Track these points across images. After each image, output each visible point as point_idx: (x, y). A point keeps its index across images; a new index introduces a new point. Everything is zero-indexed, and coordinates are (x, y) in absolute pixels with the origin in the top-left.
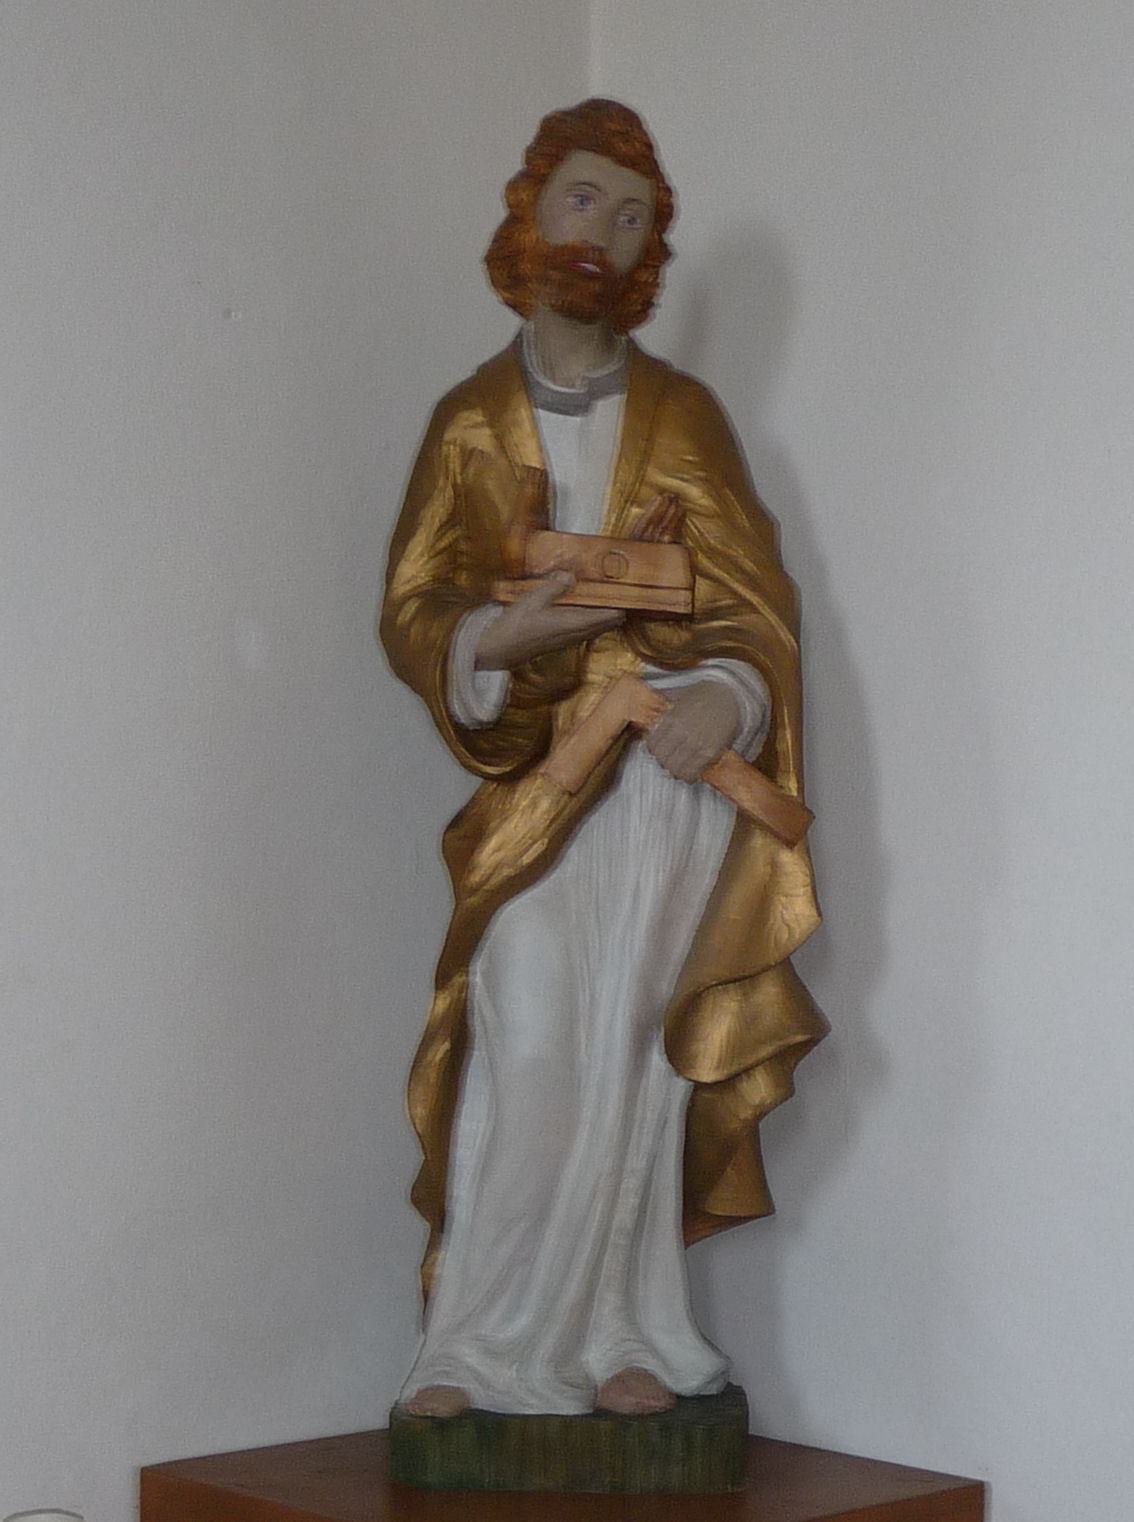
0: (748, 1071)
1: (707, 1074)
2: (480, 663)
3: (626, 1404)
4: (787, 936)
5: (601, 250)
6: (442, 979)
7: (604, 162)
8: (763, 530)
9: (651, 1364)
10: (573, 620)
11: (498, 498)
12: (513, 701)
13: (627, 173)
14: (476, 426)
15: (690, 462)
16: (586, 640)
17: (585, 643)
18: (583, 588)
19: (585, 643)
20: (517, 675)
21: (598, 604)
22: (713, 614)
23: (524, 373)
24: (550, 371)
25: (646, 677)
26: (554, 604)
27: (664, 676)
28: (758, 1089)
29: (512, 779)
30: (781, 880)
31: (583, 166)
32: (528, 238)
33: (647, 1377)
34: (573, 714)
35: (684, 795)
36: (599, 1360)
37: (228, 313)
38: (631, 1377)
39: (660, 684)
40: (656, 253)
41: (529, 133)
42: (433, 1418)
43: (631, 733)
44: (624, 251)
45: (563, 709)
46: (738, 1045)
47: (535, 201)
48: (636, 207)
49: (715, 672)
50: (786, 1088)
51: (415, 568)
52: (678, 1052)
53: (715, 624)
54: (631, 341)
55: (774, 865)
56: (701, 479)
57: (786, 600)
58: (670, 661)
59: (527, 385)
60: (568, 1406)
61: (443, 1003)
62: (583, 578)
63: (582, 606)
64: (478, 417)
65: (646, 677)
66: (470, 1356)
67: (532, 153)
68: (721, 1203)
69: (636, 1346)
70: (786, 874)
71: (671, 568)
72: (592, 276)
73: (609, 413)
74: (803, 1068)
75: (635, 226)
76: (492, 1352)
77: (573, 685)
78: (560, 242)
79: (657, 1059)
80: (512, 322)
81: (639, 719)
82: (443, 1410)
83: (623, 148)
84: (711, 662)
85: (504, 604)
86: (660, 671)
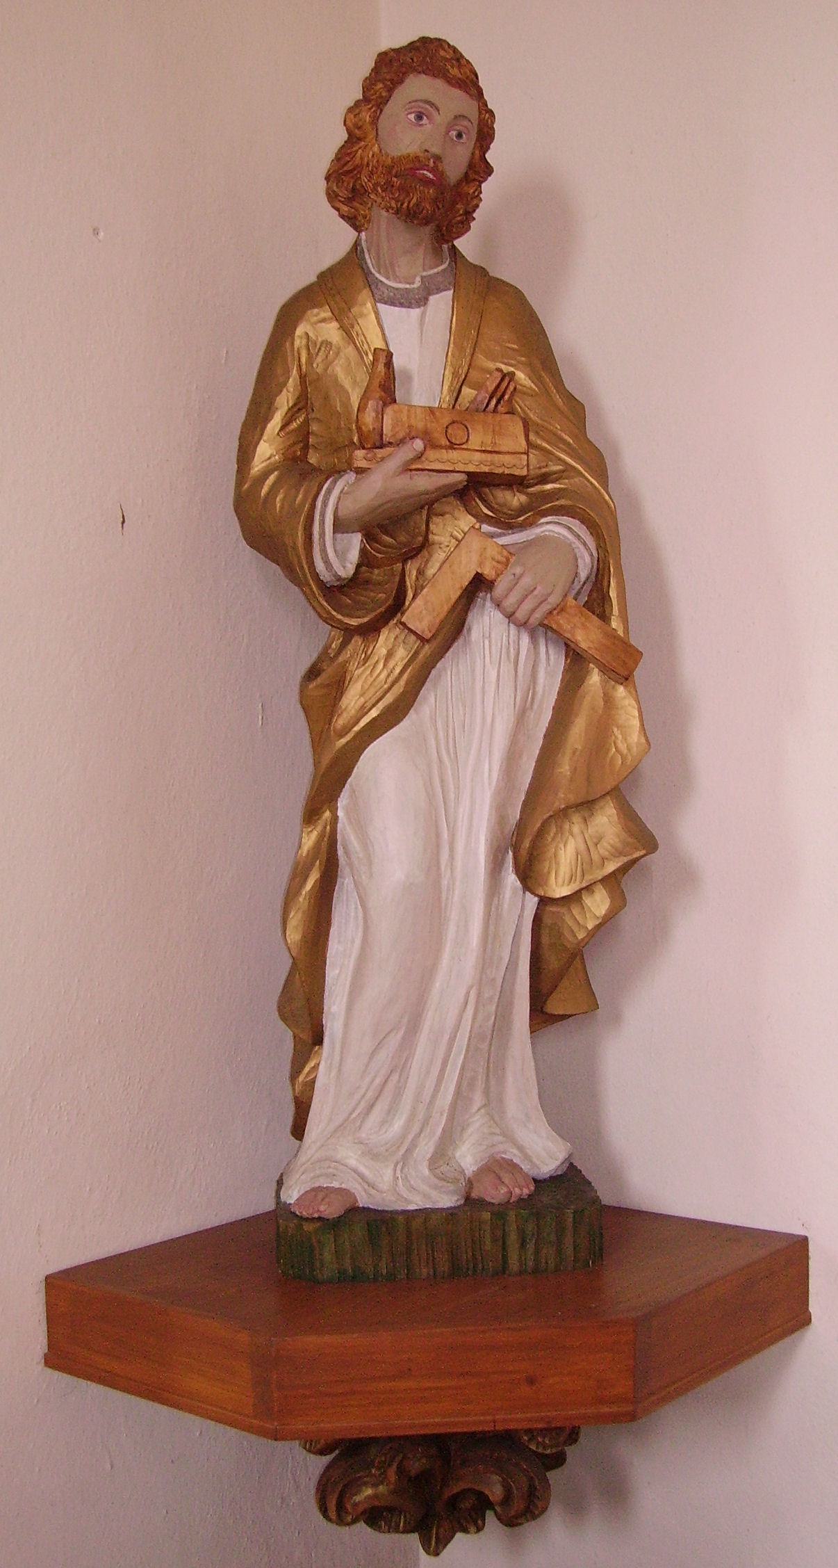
0: (589, 888)
1: (560, 890)
2: (340, 526)
3: (495, 1194)
4: (620, 762)
5: (438, 158)
6: (310, 815)
7: (439, 84)
8: (575, 411)
9: (513, 1155)
10: (424, 483)
11: (346, 383)
12: (365, 560)
13: (457, 93)
14: (324, 320)
15: (514, 350)
16: (430, 505)
17: (426, 507)
18: (431, 454)
19: (426, 507)
20: (369, 536)
21: (443, 468)
22: (544, 479)
23: (367, 274)
24: (390, 271)
25: (492, 536)
26: (407, 469)
27: (504, 535)
28: (598, 904)
29: (370, 630)
30: (620, 712)
31: (418, 87)
32: (367, 153)
33: (512, 1166)
34: (420, 572)
35: (525, 640)
36: (468, 1157)
37: (96, 232)
38: (496, 1167)
39: (503, 541)
40: (479, 169)
41: (365, 66)
42: (320, 1219)
43: (479, 585)
44: (455, 164)
45: (412, 569)
46: (585, 862)
47: (375, 121)
48: (466, 123)
49: (551, 528)
50: (619, 902)
51: (266, 451)
52: (528, 875)
53: (549, 487)
54: (454, 246)
55: (608, 700)
56: (522, 363)
57: (598, 464)
58: (506, 522)
59: (370, 283)
60: (447, 1200)
61: (309, 840)
62: (431, 444)
63: (433, 470)
64: (326, 313)
65: (492, 536)
66: (351, 1156)
67: (368, 84)
68: (554, 1007)
69: (501, 1138)
70: (617, 708)
71: (513, 438)
72: (427, 182)
73: (441, 303)
74: (627, 882)
75: (461, 141)
76: (372, 1154)
77: (420, 547)
78: (396, 153)
79: (511, 879)
80: (347, 235)
81: (488, 572)
82: (330, 1210)
83: (454, 72)
84: (549, 519)
85: (360, 471)
86: (500, 531)
